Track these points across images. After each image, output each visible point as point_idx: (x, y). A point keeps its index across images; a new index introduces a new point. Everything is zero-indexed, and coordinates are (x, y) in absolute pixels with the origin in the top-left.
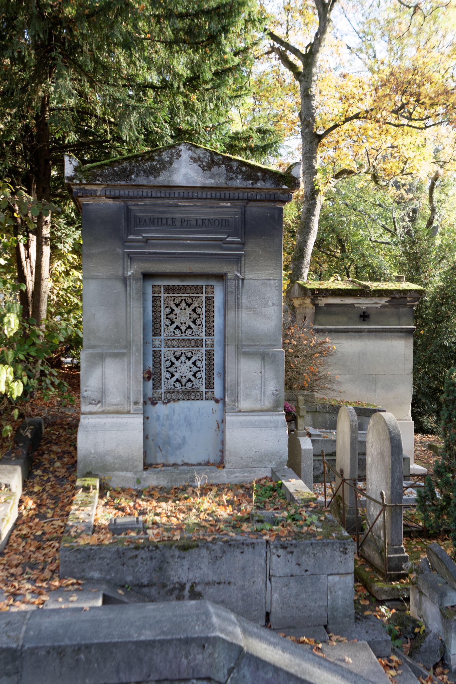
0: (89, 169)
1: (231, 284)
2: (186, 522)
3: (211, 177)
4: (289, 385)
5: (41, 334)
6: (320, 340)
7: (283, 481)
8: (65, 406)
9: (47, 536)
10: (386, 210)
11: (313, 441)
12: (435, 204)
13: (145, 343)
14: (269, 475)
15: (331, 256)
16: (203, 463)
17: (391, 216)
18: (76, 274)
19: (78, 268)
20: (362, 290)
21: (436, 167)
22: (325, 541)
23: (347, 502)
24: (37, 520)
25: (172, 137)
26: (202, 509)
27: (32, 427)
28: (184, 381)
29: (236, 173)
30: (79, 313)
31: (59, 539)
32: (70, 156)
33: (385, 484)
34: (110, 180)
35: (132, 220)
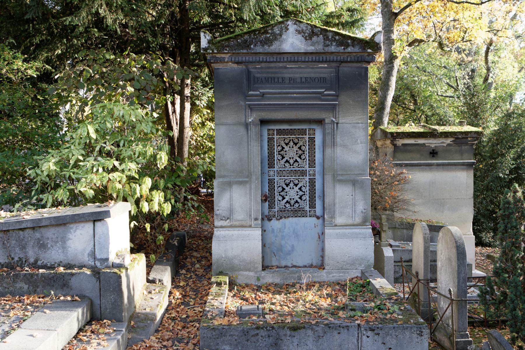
0: (219, 42)
1: (328, 127)
2: (295, 310)
3: (312, 45)
4: (374, 207)
5: (185, 168)
6: (398, 172)
7: (371, 280)
8: (202, 224)
9: (190, 318)
10: (450, 70)
11: (393, 250)
12: (490, 65)
13: (262, 173)
14: (359, 275)
15: (406, 108)
16: (307, 265)
17: (454, 75)
18: (209, 124)
19: (212, 120)
20: (431, 132)
21: (490, 35)
22: (404, 325)
23: (422, 298)
24: (182, 307)
25: (281, 16)
26: (307, 300)
27: (178, 238)
28: (292, 202)
29: (331, 41)
30: (212, 154)
31: (199, 321)
32: (205, 33)
33: (452, 283)
34: (235, 50)
35: (252, 79)
